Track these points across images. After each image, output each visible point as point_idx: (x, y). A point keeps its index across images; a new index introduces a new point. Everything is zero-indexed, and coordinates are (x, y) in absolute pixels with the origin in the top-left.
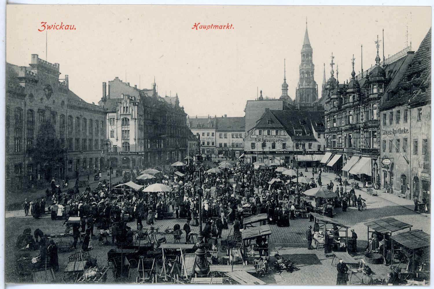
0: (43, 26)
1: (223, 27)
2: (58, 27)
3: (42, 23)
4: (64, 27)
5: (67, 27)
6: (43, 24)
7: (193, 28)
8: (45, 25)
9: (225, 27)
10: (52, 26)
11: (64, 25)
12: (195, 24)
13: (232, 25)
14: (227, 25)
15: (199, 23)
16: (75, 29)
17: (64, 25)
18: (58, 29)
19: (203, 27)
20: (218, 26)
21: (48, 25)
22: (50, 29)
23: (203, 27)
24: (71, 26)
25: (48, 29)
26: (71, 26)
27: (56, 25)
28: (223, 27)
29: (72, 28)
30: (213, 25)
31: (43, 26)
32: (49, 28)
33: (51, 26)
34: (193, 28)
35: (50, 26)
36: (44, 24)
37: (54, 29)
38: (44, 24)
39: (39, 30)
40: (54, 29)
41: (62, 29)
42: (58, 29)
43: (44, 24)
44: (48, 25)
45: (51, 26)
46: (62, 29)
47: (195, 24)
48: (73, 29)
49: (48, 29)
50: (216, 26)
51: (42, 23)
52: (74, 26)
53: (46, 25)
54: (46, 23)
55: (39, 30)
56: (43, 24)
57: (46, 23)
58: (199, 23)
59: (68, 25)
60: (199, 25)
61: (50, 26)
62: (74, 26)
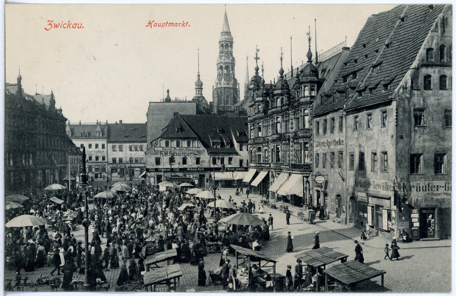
0: (50, 24)
1: (178, 24)
2: (65, 26)
3: (48, 21)
4: (71, 26)
5: (176, 25)
6: (50, 22)
7: (147, 26)
8: (51, 24)
9: (181, 25)
10: (59, 24)
11: (71, 24)
12: (150, 21)
13: (187, 23)
14: (182, 23)
15: (154, 21)
16: (83, 27)
17: (71, 24)
18: (65, 28)
19: (157, 25)
20: (173, 23)
21: (54, 24)
22: (57, 27)
23: (157, 25)
24: (79, 24)
25: (54, 27)
26: (79, 24)
27: (63, 23)
28: (178, 24)
29: (79, 26)
30: (168, 22)
31: (50, 24)
32: (56, 26)
33: (58, 25)
34: (147, 26)
35: (57, 25)
36: (50, 23)
37: (61, 27)
38: (51, 22)
39: (45, 29)
40: (61, 27)
41: (70, 27)
42: (65, 28)
43: (50, 23)
44: (54, 24)
45: (58, 25)
46: (70, 27)
47: (150, 21)
48: (80, 27)
49: (54, 27)
50: (171, 24)
51: (48, 21)
52: (81, 24)
53: (52, 24)
54: (52, 21)
55: (45, 29)
56: (50, 22)
57: (52, 21)
58: (154, 21)
59: (176, 23)
60: (153, 23)
61: (57, 25)
62: (81, 24)
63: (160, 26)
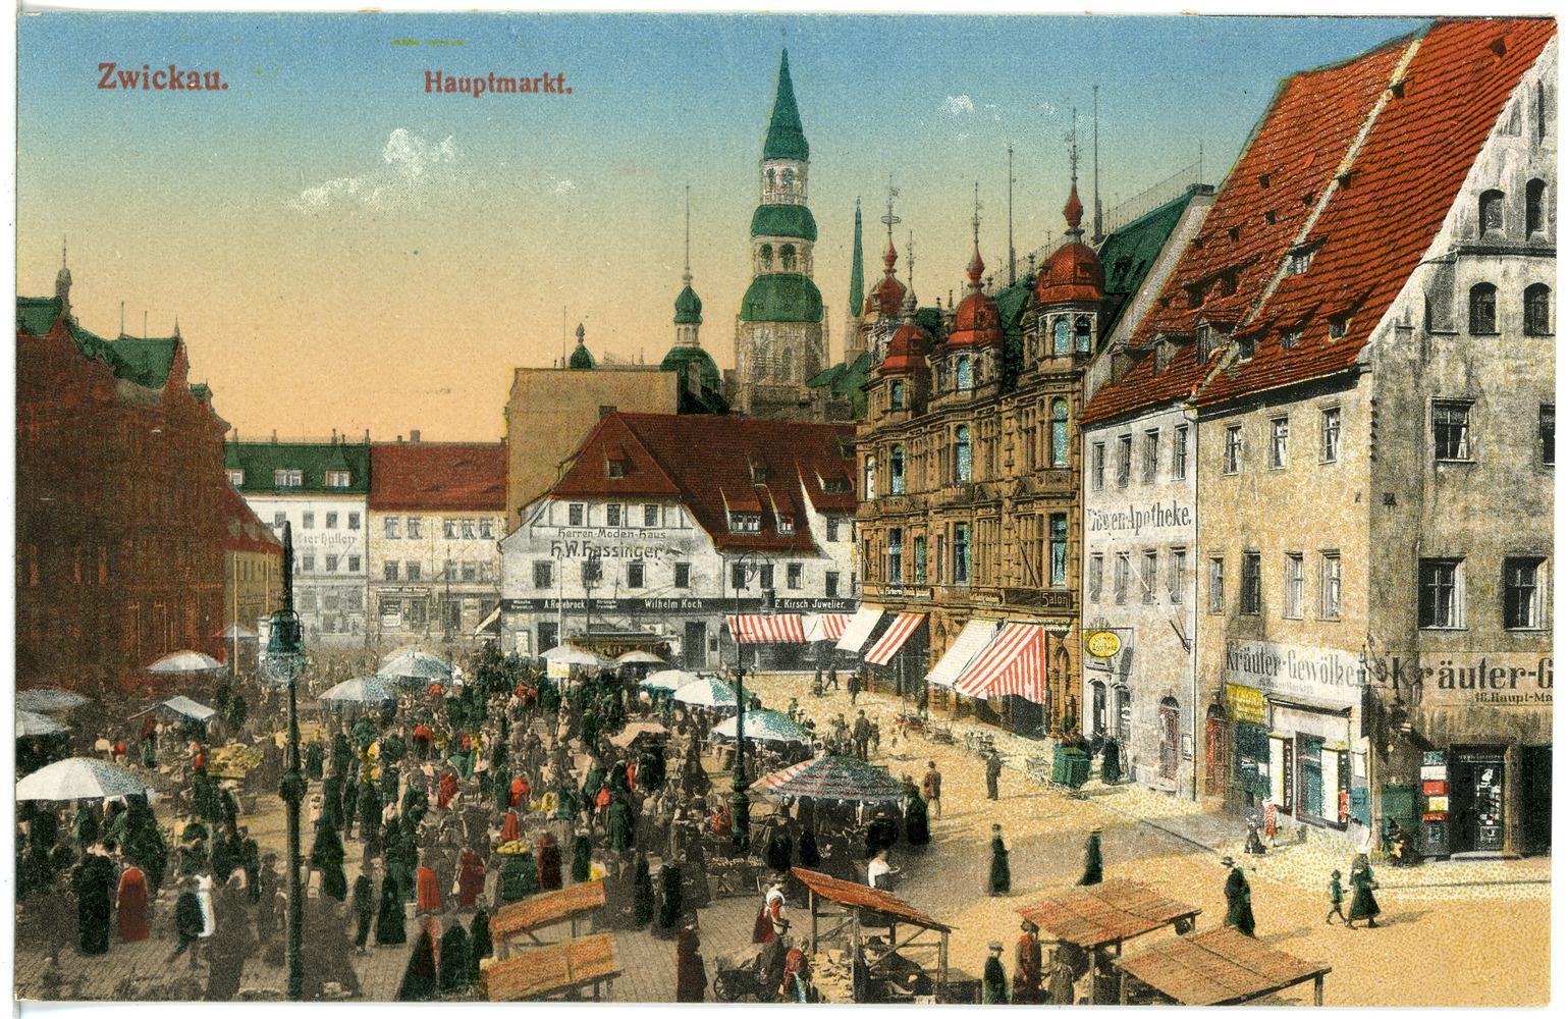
50: (507, 81)
63: (468, 89)
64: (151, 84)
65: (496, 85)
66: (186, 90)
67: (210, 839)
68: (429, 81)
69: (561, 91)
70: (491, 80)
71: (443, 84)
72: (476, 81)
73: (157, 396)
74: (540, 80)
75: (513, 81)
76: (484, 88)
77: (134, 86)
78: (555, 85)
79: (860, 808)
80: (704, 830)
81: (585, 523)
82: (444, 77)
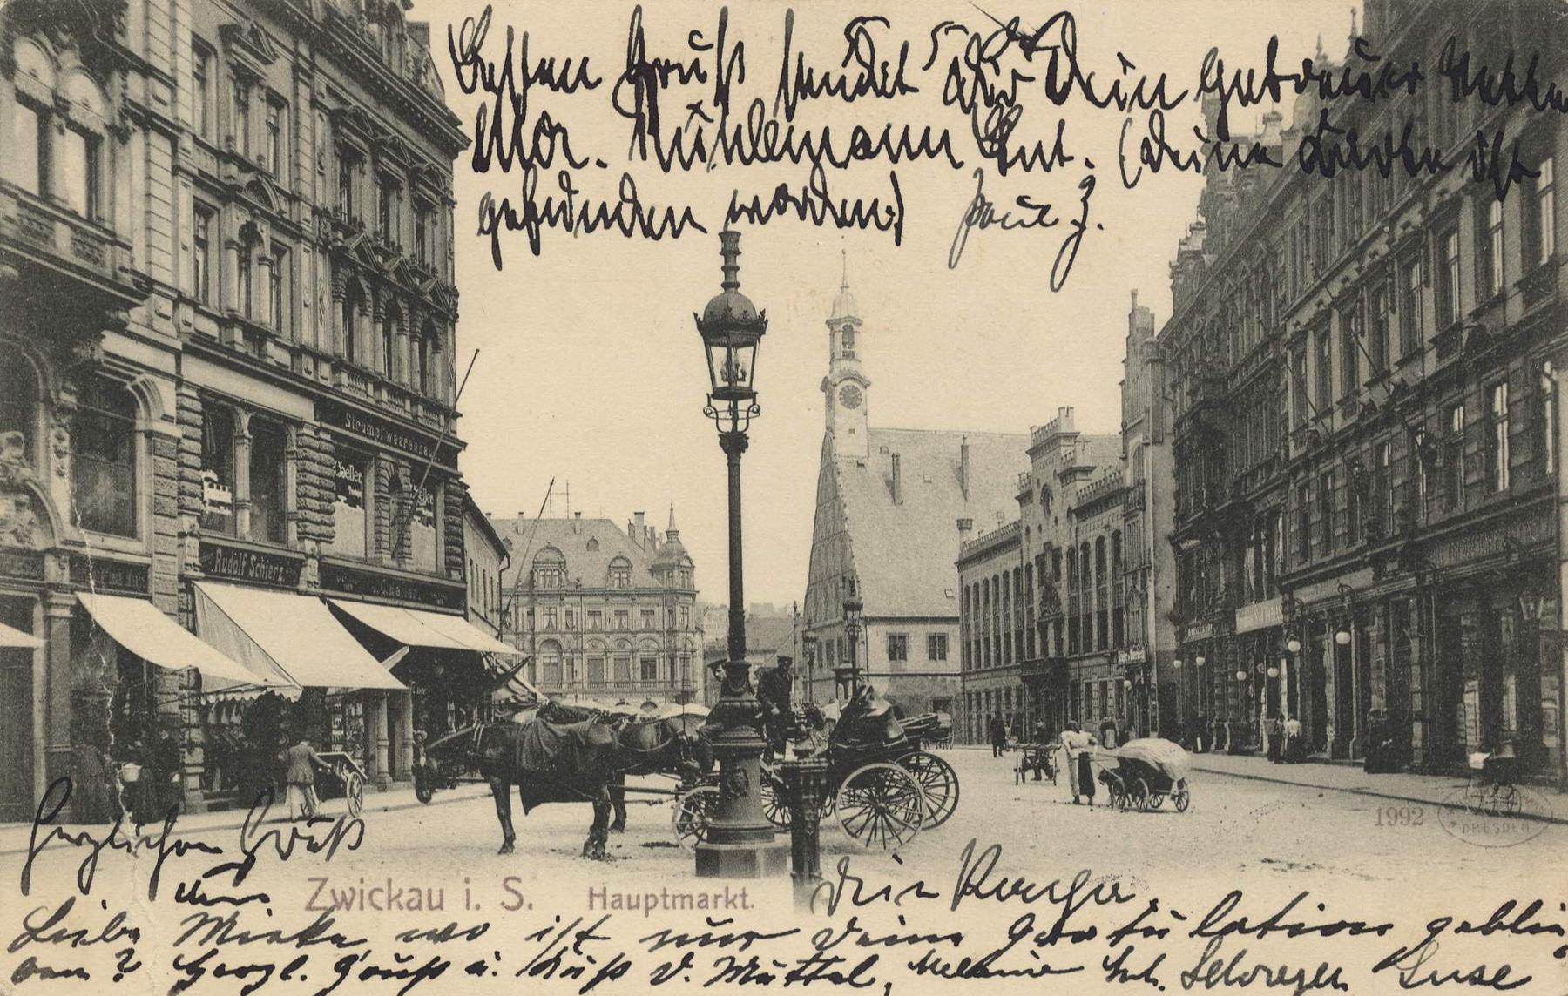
50: (683, 897)
63: (637, 906)
64: (366, 902)
65: (669, 901)
66: (405, 910)
67: (677, 710)
68: (592, 895)
69: (745, 907)
70: (665, 896)
71: (610, 900)
72: (647, 897)
73: (312, 742)
74: (720, 896)
75: (690, 897)
76: (656, 903)
77: (670, 213)
78: (739, 902)
79: (92, 582)
80: (98, 657)
81: (146, 560)
82: (609, 893)
